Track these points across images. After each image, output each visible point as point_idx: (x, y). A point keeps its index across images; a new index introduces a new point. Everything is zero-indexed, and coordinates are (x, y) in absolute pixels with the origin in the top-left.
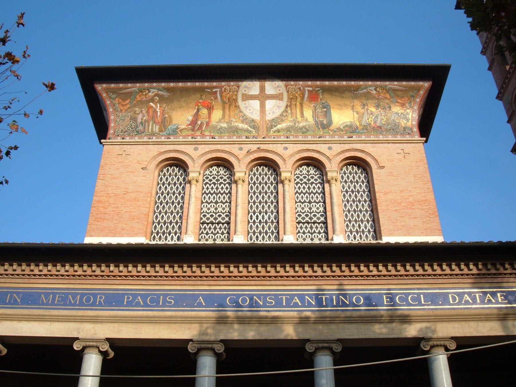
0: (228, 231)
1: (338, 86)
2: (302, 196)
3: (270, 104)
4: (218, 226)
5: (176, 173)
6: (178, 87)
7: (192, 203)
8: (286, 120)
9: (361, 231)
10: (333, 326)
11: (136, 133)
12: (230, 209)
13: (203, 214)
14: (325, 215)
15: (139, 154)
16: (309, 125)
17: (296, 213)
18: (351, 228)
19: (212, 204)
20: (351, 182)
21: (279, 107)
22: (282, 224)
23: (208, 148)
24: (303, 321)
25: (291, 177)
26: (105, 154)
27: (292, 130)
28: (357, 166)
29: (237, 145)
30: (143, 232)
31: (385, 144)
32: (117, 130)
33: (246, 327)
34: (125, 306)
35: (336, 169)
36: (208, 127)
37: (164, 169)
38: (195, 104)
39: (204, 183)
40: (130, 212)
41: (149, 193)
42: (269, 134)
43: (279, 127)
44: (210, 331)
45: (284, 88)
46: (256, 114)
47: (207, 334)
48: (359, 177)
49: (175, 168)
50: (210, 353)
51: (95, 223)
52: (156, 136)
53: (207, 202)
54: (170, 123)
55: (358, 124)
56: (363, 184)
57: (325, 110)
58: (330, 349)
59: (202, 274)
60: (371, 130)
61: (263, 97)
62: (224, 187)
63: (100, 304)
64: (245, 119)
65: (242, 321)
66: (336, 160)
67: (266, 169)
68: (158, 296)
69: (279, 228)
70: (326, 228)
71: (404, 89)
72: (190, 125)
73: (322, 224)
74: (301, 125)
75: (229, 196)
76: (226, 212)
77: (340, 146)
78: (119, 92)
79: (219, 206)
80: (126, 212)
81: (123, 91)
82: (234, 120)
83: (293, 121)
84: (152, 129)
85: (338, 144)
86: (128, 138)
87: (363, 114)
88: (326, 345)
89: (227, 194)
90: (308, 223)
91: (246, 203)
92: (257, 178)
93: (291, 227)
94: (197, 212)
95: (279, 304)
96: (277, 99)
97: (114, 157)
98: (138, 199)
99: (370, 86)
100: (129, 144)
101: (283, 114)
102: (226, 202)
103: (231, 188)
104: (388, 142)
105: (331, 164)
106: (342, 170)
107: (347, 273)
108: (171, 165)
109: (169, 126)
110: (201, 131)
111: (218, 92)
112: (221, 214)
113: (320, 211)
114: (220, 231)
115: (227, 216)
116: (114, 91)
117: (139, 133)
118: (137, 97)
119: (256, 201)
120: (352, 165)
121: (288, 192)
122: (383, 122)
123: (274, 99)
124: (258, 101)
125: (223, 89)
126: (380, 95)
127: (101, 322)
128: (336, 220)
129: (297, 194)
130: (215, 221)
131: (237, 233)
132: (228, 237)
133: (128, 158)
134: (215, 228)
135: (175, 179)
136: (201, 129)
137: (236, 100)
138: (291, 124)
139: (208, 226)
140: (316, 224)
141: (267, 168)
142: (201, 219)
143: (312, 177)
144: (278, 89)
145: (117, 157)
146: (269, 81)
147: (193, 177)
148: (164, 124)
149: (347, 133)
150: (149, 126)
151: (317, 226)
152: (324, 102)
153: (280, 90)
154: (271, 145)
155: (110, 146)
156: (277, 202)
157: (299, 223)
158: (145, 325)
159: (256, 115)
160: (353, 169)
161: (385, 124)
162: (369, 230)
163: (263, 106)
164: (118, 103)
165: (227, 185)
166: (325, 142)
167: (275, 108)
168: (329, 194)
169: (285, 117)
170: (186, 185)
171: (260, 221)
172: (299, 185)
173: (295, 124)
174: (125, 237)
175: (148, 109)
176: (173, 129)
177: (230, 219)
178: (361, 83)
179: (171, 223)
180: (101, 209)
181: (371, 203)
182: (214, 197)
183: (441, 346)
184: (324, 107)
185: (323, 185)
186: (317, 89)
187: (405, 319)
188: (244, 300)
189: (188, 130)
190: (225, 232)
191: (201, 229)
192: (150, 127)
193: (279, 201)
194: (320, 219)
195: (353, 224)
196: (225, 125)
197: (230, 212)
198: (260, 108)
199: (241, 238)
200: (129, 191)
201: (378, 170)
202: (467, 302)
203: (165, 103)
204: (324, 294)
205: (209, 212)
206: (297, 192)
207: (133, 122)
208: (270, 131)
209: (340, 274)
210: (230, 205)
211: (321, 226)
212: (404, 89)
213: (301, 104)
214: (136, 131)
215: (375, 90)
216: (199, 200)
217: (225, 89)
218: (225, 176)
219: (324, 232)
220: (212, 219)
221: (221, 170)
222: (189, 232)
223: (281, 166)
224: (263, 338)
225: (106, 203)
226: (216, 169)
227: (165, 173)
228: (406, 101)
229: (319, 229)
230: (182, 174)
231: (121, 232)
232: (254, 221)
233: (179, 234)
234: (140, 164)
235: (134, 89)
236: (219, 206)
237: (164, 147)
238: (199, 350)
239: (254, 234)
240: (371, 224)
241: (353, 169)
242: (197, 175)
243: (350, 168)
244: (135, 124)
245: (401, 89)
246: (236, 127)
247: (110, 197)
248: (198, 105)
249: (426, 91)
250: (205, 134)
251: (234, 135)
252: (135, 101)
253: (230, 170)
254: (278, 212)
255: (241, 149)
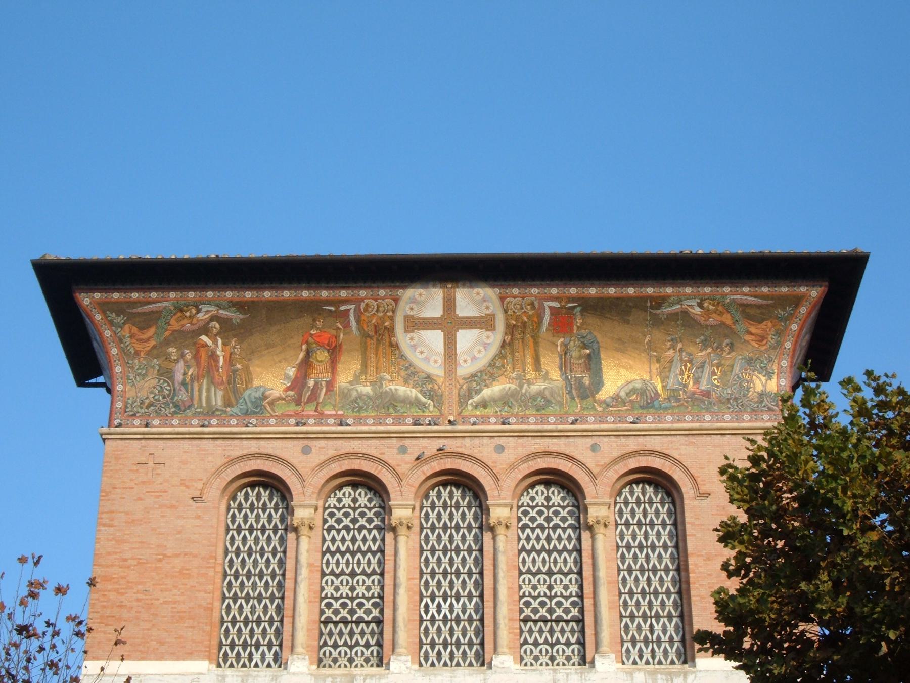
0: (378, 640)
1: (618, 299)
2: (534, 558)
3: (465, 339)
4: (357, 628)
5: (265, 504)
6: (261, 301)
7: (302, 580)
8: (503, 377)
9: (654, 639)
11: (174, 409)
12: (382, 588)
13: (326, 600)
14: (580, 602)
15: (184, 463)
16: (551, 388)
17: (521, 598)
18: (633, 634)
19: (344, 578)
20: (639, 524)
22: (489, 627)
25: (509, 518)
26: (110, 462)
27: (515, 403)
28: (653, 486)
29: (394, 441)
30: (204, 649)
31: (715, 436)
32: (130, 401)
35: (607, 500)
36: (332, 393)
37: (239, 493)
38: (301, 339)
39: (326, 527)
40: (175, 602)
41: (211, 557)
42: (465, 413)
43: (486, 392)
45: (497, 302)
46: (436, 361)
48: (657, 513)
49: (262, 490)
51: (103, 629)
52: (217, 416)
53: (332, 573)
54: (246, 383)
55: (659, 387)
56: (664, 529)
57: (588, 351)
60: (687, 402)
62: (369, 538)
64: (411, 374)
66: (608, 478)
67: (457, 493)
69: (483, 585)
70: (583, 632)
71: (765, 302)
72: (292, 390)
73: (574, 624)
74: (535, 388)
75: (379, 559)
76: (373, 597)
77: (616, 442)
78: (131, 311)
79: (358, 582)
80: (165, 602)
81: (140, 310)
82: (388, 377)
83: (516, 379)
84: (208, 398)
85: (613, 439)
86: (156, 422)
87: (671, 361)
89: (374, 554)
90: (545, 621)
91: (415, 579)
92: (439, 516)
93: (510, 633)
94: (313, 600)
96: (481, 328)
97: (131, 470)
98: (187, 572)
99: (689, 297)
100: (160, 437)
101: (495, 363)
102: (374, 572)
103: (383, 540)
105: (597, 488)
106: (619, 494)
109: (244, 390)
110: (315, 403)
112: (363, 600)
113: (571, 593)
114: (362, 639)
115: (375, 605)
116: (119, 308)
117: (180, 409)
118: (171, 323)
119: (437, 571)
120: (643, 484)
121: (504, 552)
122: (715, 380)
123: (475, 328)
124: (440, 331)
125: (363, 305)
126: (710, 318)
128: (601, 620)
129: (524, 554)
130: (352, 617)
132: (378, 652)
133: (159, 471)
134: (351, 634)
135: (264, 518)
136: (316, 399)
137: (391, 331)
138: (513, 386)
139: (336, 629)
140: (561, 624)
141: (460, 491)
142: (322, 612)
143: (556, 513)
144: (485, 304)
145: (137, 471)
146: (464, 286)
147: (302, 519)
148: (233, 387)
149: (633, 409)
150: (200, 390)
151: (562, 627)
152: (584, 332)
153: (487, 308)
154: (468, 440)
155: (119, 442)
156: (481, 574)
157: (526, 620)
159: (436, 366)
160: (644, 494)
161: (717, 386)
162: (671, 637)
164: (128, 335)
165: (375, 532)
166: (585, 434)
167: (478, 347)
168: (591, 557)
170: (289, 535)
171: (445, 616)
172: (528, 531)
173: (521, 386)
174: (166, 660)
175: (198, 351)
176: (253, 400)
177: (382, 612)
178: (669, 290)
180: (112, 596)
181: (679, 575)
182: (348, 560)
184: (585, 346)
185: (578, 530)
186: (570, 305)
189: (288, 402)
190: (372, 642)
191: (321, 634)
192: (204, 394)
193: (485, 616)
194: (570, 612)
195: (639, 624)
196: (367, 389)
197: (382, 595)
198: (445, 349)
199: (407, 661)
200: (169, 552)
201: (696, 503)
203: (235, 336)
205: (338, 595)
206: (523, 549)
207: (165, 381)
208: (467, 405)
210: (382, 580)
211: (573, 627)
212: (765, 302)
213: (535, 340)
214: (173, 403)
215: (700, 305)
216: (317, 571)
217: (367, 304)
220: (344, 613)
221: (360, 494)
222: (299, 649)
223: (489, 493)
225: (122, 582)
226: (350, 494)
228: (768, 330)
230: (276, 504)
231: (157, 649)
233: (277, 648)
234: (188, 487)
236: (358, 582)
237: (236, 446)
240: (677, 623)
241: (644, 494)
242: (311, 513)
243: (638, 489)
244: (169, 385)
245: (757, 303)
246: (393, 394)
247: (129, 567)
248: (307, 342)
250: (326, 413)
251: (388, 415)
252: (166, 330)
253: (380, 496)
254: (481, 596)
255: (403, 450)
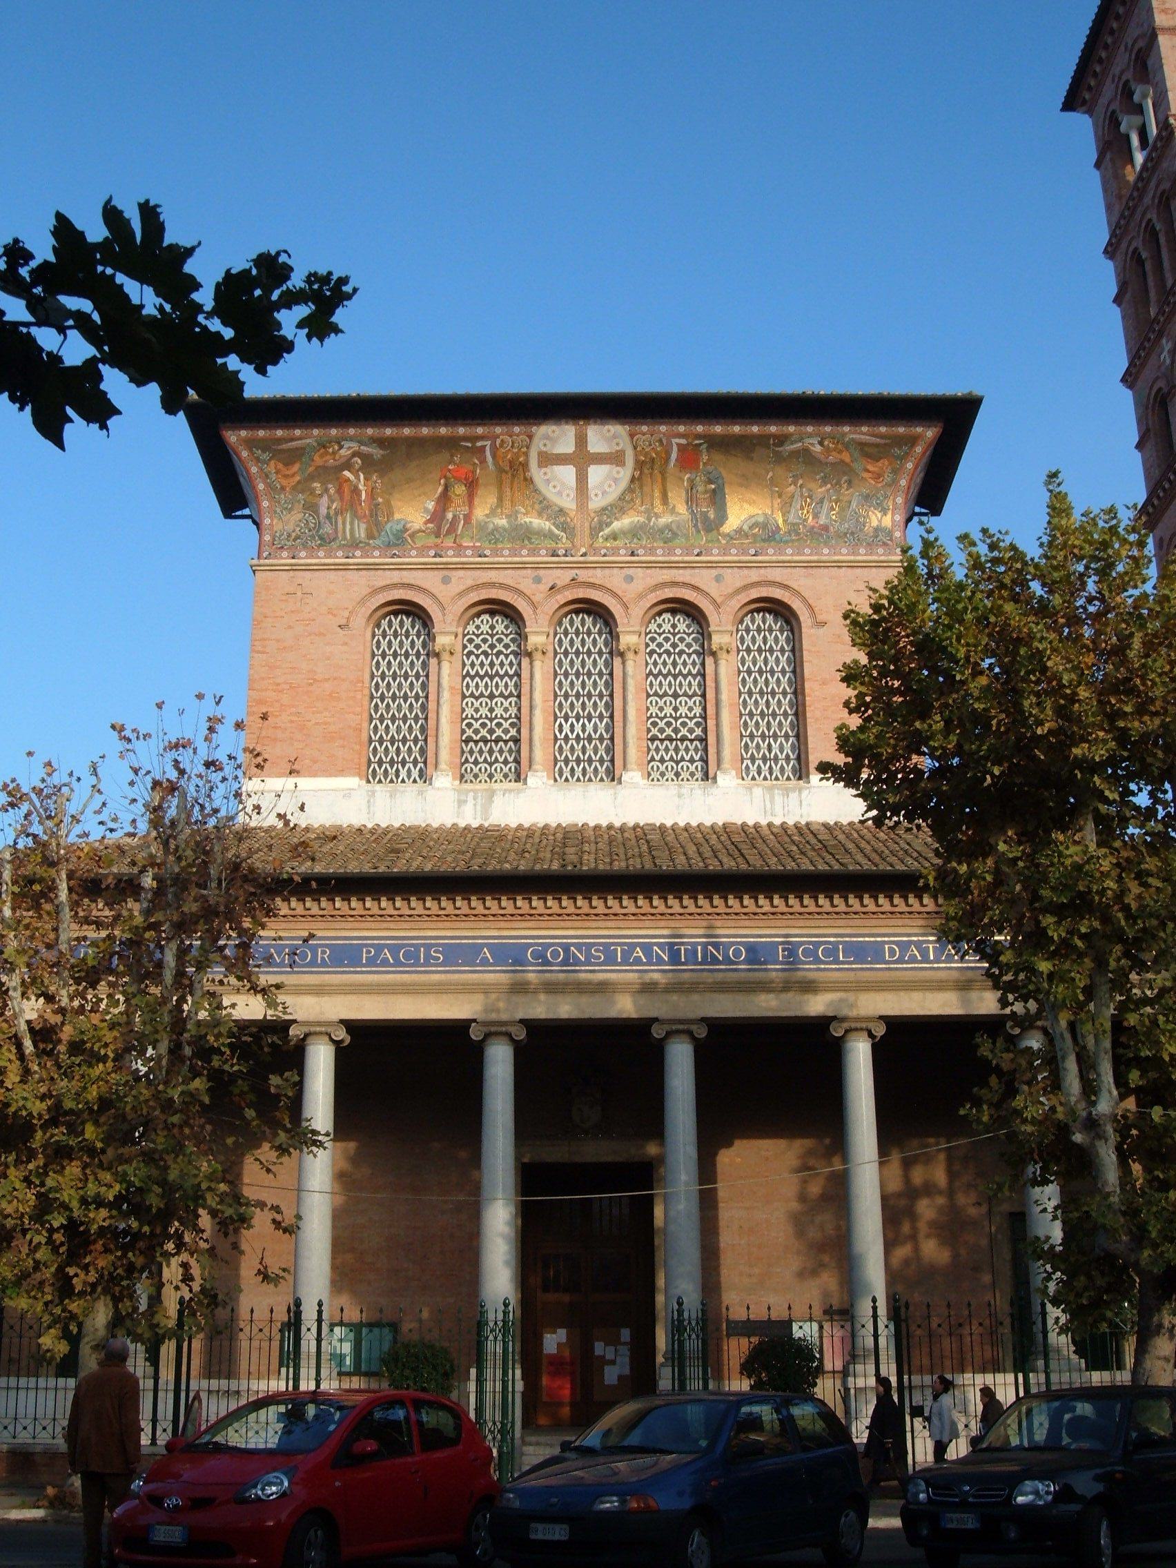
1: (743, 436)
3: (596, 474)
5: (407, 631)
10: (695, 997)
12: (519, 709)
15: (331, 593)
17: (648, 718)
21: (616, 480)
23: (470, 578)
24: (648, 988)
29: (529, 571)
33: (559, 998)
34: (364, 966)
40: (326, 724)
41: (359, 681)
42: (596, 545)
43: (616, 525)
44: (501, 1005)
45: (627, 439)
47: (498, 1011)
50: (505, 1039)
53: (472, 695)
58: (690, 1033)
59: (487, 912)
61: (582, 459)
62: (506, 662)
63: (324, 964)
65: (552, 988)
68: (417, 947)
70: (706, 750)
74: (663, 521)
76: (510, 717)
80: (317, 724)
81: (284, 446)
82: (523, 510)
84: (352, 530)
87: (793, 497)
88: (681, 1027)
89: (511, 677)
95: (610, 959)
99: (810, 435)
100: (307, 569)
104: (839, 565)
106: (741, 622)
107: (722, 909)
108: (396, 613)
111: (488, 448)
116: (265, 446)
127: (329, 993)
131: (534, 767)
134: (491, 752)
137: (525, 466)
138: (642, 519)
142: (463, 732)
145: (286, 601)
146: (595, 423)
149: (755, 542)
150: (344, 524)
154: (599, 571)
156: (611, 696)
158: (400, 996)
160: (764, 622)
163: (582, 479)
166: (710, 565)
169: (628, 502)
173: (649, 519)
177: (519, 731)
179: (404, 741)
183: (862, 1029)
187: (809, 987)
188: (555, 954)
189: (429, 534)
190: (511, 759)
191: (463, 752)
192: (348, 527)
196: (502, 522)
201: (813, 631)
202: (913, 959)
204: (682, 944)
206: (651, 673)
209: (711, 910)
212: (883, 441)
215: (821, 443)
218: (507, 636)
219: (701, 759)
222: (443, 766)
224: (586, 1016)
227: (384, 631)
229: (692, 752)
230: (419, 631)
232: (566, 737)
234: (335, 615)
235: (308, 441)
238: (488, 1035)
239: (567, 763)
241: (764, 622)
248: (445, 477)
249: (930, 445)
251: (522, 547)
